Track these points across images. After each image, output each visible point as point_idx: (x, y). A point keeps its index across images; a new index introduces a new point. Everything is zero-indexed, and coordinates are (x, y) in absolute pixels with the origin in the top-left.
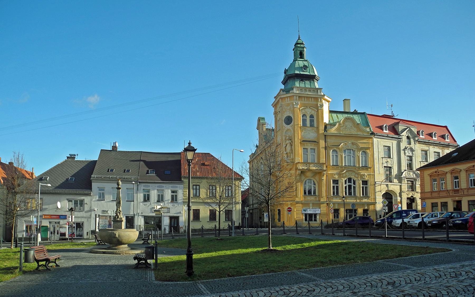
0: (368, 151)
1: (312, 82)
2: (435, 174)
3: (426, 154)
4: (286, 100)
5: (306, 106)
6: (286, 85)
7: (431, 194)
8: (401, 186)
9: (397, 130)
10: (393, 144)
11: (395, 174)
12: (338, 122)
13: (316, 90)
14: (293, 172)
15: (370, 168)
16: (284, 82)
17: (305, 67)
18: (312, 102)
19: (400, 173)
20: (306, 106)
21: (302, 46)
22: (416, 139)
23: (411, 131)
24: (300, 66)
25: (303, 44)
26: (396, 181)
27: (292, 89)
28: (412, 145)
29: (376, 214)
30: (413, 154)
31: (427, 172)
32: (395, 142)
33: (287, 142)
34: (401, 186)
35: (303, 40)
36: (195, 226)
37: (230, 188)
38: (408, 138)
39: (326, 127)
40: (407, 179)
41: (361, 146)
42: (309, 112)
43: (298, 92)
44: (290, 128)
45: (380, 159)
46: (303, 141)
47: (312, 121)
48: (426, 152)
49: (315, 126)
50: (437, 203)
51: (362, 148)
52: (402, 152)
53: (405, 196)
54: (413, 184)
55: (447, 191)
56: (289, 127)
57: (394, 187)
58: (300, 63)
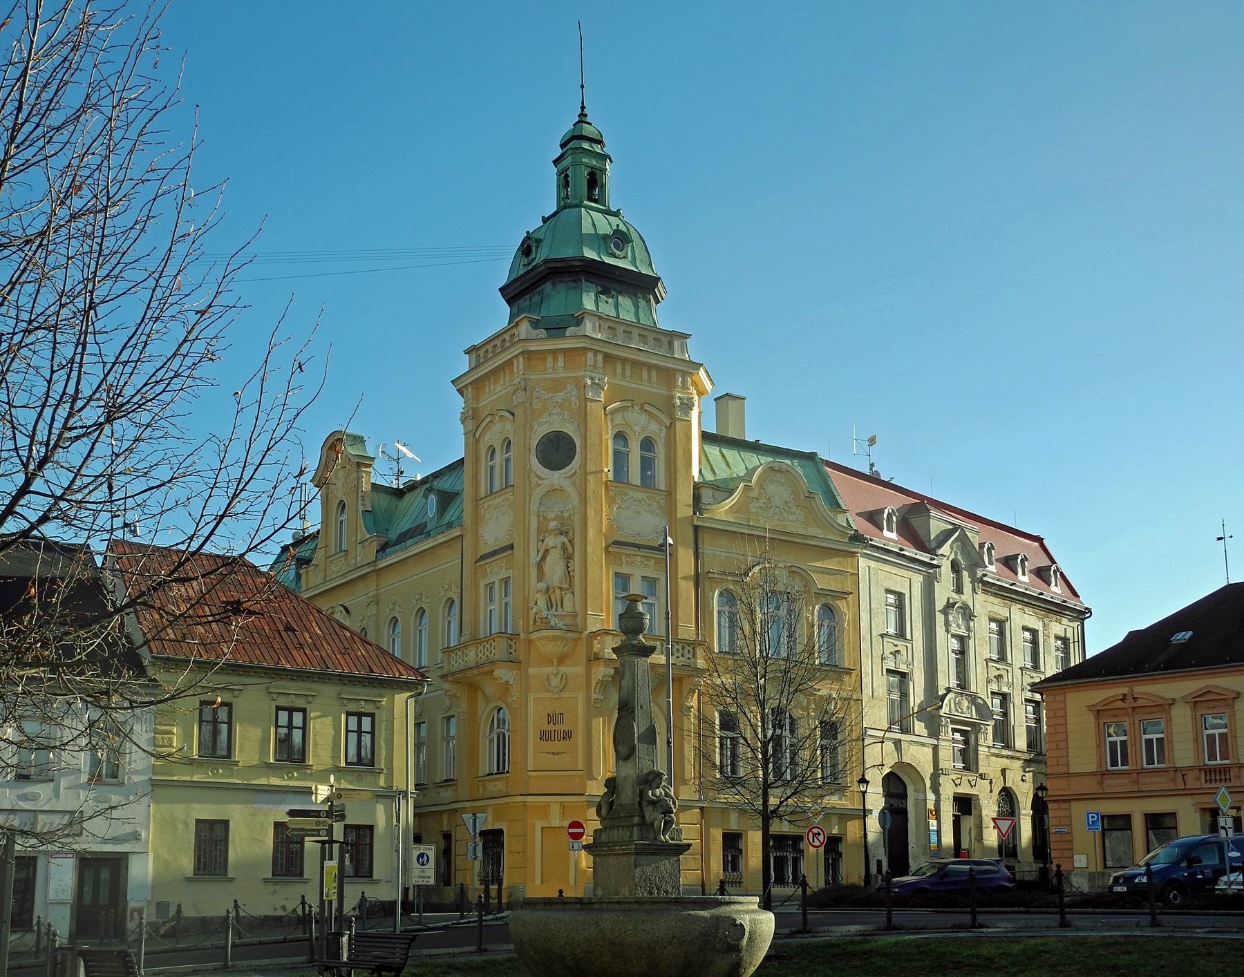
0: (842, 605)
1: (642, 303)
2: (1120, 704)
3: (1001, 633)
4: (550, 359)
5: (629, 401)
6: (524, 302)
7: (1101, 783)
8: (935, 748)
9: (921, 532)
10: (911, 583)
11: (918, 701)
12: (742, 479)
13: (665, 340)
14: (575, 669)
15: (848, 672)
16: (515, 293)
17: (621, 238)
18: (651, 386)
19: (934, 697)
20: (629, 401)
21: (597, 148)
22: (979, 573)
23: (964, 541)
24: (601, 232)
25: (600, 142)
26: (919, 727)
27: (579, 321)
28: (967, 597)
29: (867, 856)
30: (968, 629)
31: (1080, 701)
32: (918, 580)
33: (551, 541)
34: (935, 748)
35: (597, 124)
36: (212, 902)
37: (366, 723)
38: (955, 567)
39: (697, 499)
40: (953, 722)
41: (821, 582)
42: (640, 424)
43: (599, 336)
44: (566, 484)
45: (877, 641)
46: (616, 543)
47: (647, 464)
48: (1001, 623)
49: (661, 483)
50: (1127, 818)
51: (822, 593)
52: (940, 618)
53: (948, 790)
54: (966, 742)
55: (1176, 770)
56: (556, 478)
57: (919, 756)
58: (593, 221)
